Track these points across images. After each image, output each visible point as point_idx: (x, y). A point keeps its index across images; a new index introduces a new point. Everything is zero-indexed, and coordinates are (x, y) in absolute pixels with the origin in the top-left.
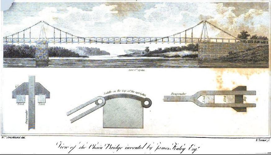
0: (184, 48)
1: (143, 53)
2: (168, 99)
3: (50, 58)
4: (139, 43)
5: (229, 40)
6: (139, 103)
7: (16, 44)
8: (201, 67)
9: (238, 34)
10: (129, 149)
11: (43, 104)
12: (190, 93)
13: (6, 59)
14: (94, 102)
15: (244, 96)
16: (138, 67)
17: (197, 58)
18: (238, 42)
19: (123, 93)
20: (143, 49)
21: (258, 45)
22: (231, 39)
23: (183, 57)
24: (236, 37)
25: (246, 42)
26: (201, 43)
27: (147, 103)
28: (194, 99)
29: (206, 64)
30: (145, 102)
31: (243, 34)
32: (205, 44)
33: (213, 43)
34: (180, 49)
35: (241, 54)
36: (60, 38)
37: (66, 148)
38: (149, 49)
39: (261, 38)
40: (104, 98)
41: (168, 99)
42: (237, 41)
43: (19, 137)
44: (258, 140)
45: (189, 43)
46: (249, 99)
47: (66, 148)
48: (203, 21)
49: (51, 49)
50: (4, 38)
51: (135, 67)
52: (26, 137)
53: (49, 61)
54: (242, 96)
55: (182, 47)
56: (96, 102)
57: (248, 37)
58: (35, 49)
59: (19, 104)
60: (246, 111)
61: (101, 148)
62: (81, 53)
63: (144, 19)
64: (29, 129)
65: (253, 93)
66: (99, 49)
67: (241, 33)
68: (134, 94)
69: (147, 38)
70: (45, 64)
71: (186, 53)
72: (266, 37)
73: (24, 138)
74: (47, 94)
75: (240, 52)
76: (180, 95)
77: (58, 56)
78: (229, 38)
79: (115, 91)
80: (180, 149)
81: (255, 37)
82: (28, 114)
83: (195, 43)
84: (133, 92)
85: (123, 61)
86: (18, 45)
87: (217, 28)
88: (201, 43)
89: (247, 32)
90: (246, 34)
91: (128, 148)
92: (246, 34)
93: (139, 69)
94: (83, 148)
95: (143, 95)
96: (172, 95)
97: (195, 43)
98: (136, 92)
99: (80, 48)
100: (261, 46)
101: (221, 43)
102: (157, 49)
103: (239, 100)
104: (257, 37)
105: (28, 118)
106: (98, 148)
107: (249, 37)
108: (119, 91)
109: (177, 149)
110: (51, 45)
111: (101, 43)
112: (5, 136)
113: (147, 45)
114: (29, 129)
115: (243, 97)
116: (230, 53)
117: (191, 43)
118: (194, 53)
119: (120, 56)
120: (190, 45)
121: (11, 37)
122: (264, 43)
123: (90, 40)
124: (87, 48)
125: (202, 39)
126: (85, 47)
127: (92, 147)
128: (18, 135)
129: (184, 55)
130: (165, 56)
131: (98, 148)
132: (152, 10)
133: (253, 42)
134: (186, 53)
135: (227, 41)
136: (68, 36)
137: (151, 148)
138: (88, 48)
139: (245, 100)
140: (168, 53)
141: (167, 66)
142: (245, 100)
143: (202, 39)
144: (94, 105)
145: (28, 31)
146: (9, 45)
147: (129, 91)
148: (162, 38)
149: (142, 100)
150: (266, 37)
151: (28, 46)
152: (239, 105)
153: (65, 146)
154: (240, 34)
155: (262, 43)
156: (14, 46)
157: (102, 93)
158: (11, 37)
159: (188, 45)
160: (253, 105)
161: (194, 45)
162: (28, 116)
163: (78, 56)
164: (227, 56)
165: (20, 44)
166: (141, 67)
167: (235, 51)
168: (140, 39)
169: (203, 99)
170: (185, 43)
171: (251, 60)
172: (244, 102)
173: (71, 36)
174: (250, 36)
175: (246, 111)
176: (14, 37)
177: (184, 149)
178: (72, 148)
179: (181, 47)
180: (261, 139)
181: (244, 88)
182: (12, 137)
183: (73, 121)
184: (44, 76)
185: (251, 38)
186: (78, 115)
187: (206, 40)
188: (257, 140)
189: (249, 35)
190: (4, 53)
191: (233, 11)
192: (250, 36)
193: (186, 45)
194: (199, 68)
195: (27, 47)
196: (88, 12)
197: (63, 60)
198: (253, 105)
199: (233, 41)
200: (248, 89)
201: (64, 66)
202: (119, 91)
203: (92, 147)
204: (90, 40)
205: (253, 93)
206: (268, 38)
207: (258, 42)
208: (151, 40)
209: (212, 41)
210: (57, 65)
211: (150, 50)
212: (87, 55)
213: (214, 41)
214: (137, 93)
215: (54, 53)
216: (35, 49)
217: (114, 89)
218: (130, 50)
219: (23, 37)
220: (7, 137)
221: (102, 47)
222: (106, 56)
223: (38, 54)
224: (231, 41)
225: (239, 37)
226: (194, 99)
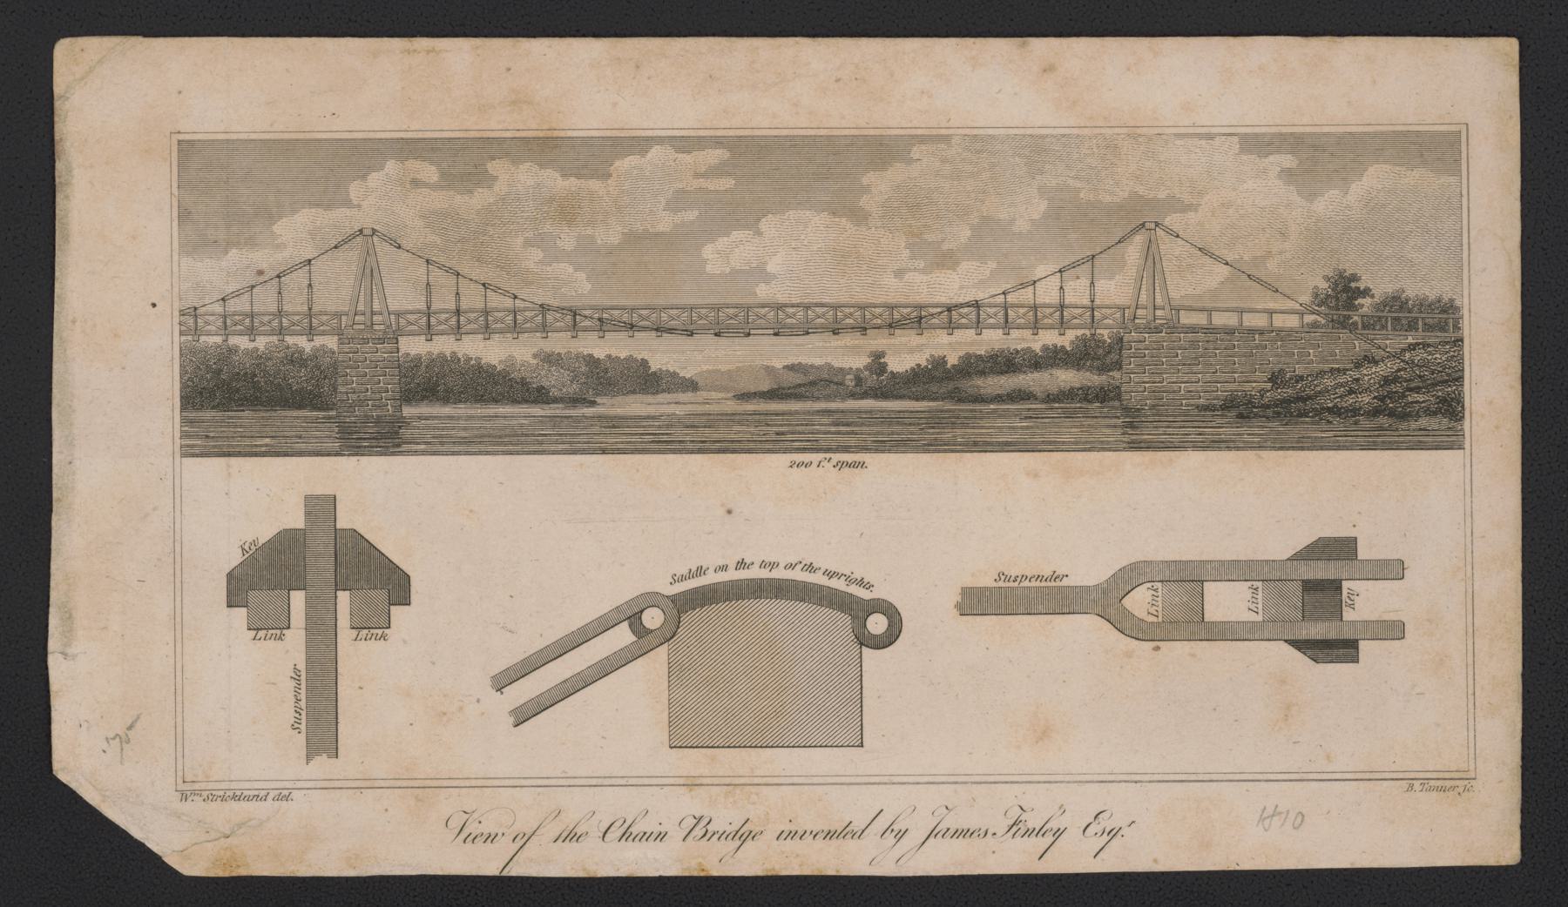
0: (1055, 358)
1: (859, 380)
2: (975, 602)
3: (407, 411)
4: (835, 332)
5: (1271, 313)
6: (844, 620)
7: (242, 342)
8: (1135, 446)
9: (1312, 284)
10: (797, 837)
11: (380, 632)
12: (1089, 572)
13: (192, 415)
14: (626, 624)
15: (1345, 584)
16: (828, 450)
17: (1117, 403)
18: (1315, 325)
19: (765, 574)
20: (859, 362)
21: (1410, 340)
22: (1282, 312)
23: (1050, 398)
24: (1306, 298)
25: (1355, 324)
26: (1137, 328)
27: (877, 624)
28: (1105, 603)
29: (1161, 431)
30: (869, 621)
31: (1336, 284)
32: (1155, 337)
33: (1193, 329)
34: (1037, 363)
35: (1328, 382)
36: (458, 312)
37: (491, 838)
38: (885, 364)
39: (1423, 305)
40: (673, 599)
41: (975, 602)
42: (1309, 318)
43: (263, 793)
44: (1417, 784)
45: (1080, 332)
46: (1367, 601)
47: (491, 838)
48: (1143, 225)
49: (417, 361)
50: (182, 313)
51: (818, 450)
52: (295, 794)
53: (402, 422)
54: (1336, 586)
55: (1045, 348)
56: (635, 620)
57: (1360, 301)
58: (335, 365)
59: (262, 633)
60: (1355, 660)
61: (661, 836)
62: (554, 380)
63: (859, 216)
64: (309, 759)
65: (1392, 570)
66: (644, 363)
67: (1327, 278)
68: (818, 579)
69: (1077, 307)
70: (387, 438)
71: (1066, 378)
72: (1452, 300)
73: (287, 798)
74: (397, 586)
75: (1321, 373)
76: (1038, 584)
77: (446, 401)
78: (1271, 305)
79: (724, 568)
80: (1041, 832)
81: (1396, 302)
82: (303, 686)
83: (1105, 332)
84: (810, 568)
85: (763, 418)
86: (252, 345)
87: (1212, 256)
88: (1137, 328)
89: (1354, 278)
90: (1353, 285)
91: (792, 835)
92: (1353, 285)
93: (836, 457)
94: (572, 836)
95: (861, 583)
96: (1001, 584)
97: (1105, 332)
98: (763, 565)
99: (550, 359)
100: (1425, 345)
101: (1230, 331)
102: (924, 363)
103: (1318, 605)
104: (1407, 301)
105: (303, 704)
106: (645, 836)
107: (1366, 302)
108: (741, 564)
109: (1028, 833)
110: (414, 346)
111: (654, 334)
112: (194, 793)
113: (878, 341)
114: (309, 759)
115: (1340, 588)
116: (1275, 379)
117: (1087, 332)
118: (1093, 379)
119: (744, 397)
120: (1083, 340)
121: (218, 308)
122: (1443, 329)
123: (600, 320)
124: (592, 361)
125: (1139, 312)
126: (577, 356)
127: (615, 833)
128: (247, 785)
129: (1055, 390)
130: (957, 396)
131: (645, 836)
132: (896, 174)
133: (1384, 327)
134: (1066, 378)
135: (1259, 321)
136: (495, 300)
137: (900, 835)
138: (591, 356)
139: (1352, 606)
140: (979, 382)
141: (975, 444)
142: (1352, 606)
143: (1139, 312)
144: (623, 636)
145: (300, 277)
146: (205, 350)
147: (791, 566)
148: (949, 310)
149: (858, 610)
150: (1452, 300)
151: (301, 352)
152: (1316, 630)
153: (488, 827)
154: (1323, 285)
155: (1429, 328)
156: (233, 350)
157: (658, 574)
158: (218, 308)
159: (1072, 342)
160: (1393, 630)
161: (1099, 343)
162: (303, 696)
163: (540, 396)
164: (1263, 392)
165: (261, 343)
166: (846, 449)
167: (1300, 370)
168: (868, 316)
169: (1165, 605)
170: (973, 331)
171: (1376, 412)
172: (1348, 615)
173: (509, 303)
174: (1373, 296)
175: (1355, 660)
176: (234, 305)
177: (1059, 833)
178: (519, 842)
179: (1037, 347)
180: (1432, 783)
181: (1343, 549)
182: (230, 793)
183: (522, 716)
184: (381, 494)
185: (1377, 307)
186: (538, 683)
187: (1159, 313)
188: (1412, 786)
189: (1366, 292)
190: (184, 386)
191: (1287, 175)
192: (1373, 296)
193: (1067, 340)
194: (1124, 449)
195: (296, 359)
196: (594, 185)
197: (470, 418)
198: (1393, 630)
199: (1292, 322)
200: (1363, 553)
201: (475, 448)
202: (741, 564)
203: (615, 833)
204: (600, 320)
205: (1392, 570)
206: (1458, 303)
207: (1412, 326)
208: (897, 316)
209: (1187, 319)
210: (442, 444)
211: (889, 369)
212: (590, 396)
213: (1199, 319)
214: (830, 575)
215: (432, 383)
216: (335, 365)
217: (716, 554)
218: (791, 368)
219: (1086, 302)
220: (205, 794)
221: (663, 355)
222: (682, 397)
223: (349, 386)
224: (1279, 321)
225: (1321, 300)
226: (1105, 603)
